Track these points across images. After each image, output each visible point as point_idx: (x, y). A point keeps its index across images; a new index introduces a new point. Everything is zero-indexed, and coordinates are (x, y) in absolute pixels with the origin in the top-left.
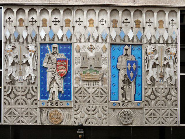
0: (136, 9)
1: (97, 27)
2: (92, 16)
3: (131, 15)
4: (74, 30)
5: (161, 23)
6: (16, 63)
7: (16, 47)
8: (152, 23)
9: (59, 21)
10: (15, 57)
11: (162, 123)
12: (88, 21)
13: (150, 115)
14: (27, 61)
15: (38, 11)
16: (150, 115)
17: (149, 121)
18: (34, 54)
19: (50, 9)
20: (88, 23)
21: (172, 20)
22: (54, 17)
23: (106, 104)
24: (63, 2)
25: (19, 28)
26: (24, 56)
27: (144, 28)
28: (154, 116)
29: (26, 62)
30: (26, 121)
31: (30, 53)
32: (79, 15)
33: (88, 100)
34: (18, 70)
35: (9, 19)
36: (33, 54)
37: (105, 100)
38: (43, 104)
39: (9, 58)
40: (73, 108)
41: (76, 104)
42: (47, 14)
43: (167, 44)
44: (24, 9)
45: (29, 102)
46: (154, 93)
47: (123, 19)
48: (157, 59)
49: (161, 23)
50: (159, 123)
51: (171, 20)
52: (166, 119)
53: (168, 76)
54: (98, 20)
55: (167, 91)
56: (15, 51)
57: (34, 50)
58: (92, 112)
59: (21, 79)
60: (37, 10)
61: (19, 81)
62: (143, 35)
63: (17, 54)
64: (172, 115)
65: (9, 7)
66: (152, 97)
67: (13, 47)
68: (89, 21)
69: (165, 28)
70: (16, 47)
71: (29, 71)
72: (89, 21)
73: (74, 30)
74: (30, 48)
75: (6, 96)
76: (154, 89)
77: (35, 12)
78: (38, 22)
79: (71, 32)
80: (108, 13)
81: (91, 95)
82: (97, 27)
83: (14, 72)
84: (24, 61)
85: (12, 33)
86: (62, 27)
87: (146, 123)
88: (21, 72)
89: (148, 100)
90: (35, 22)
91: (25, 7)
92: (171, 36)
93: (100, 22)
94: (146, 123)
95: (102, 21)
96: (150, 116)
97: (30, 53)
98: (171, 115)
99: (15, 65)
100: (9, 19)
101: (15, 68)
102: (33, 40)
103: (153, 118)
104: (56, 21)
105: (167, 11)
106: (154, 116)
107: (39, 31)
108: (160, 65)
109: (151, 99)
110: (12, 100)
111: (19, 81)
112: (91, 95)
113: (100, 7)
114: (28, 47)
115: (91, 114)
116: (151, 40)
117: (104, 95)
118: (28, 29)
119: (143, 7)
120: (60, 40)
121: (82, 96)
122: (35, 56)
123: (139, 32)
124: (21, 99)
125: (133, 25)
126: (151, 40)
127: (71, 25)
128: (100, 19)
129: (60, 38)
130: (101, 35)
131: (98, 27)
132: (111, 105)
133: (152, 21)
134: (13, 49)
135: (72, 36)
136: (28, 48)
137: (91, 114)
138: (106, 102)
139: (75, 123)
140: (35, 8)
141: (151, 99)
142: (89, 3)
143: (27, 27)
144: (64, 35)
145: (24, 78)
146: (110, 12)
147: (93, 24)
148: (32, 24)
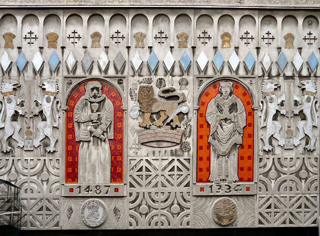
0: (309, 14)
1: (237, 48)
2: (96, 27)
3: (171, 23)
4: (63, 53)
5: (226, 37)
6: (21, 115)
7: (20, 86)
8: (166, 38)
9: (315, 39)
10: (18, 105)
11: (291, 222)
12: (219, 37)
13: (298, 208)
14: (41, 112)
15: (107, 17)
16: (298, 208)
17: (296, 218)
18: (55, 98)
19: (237, 14)
20: (284, 41)
21: (310, 34)
22: (267, 28)
23: (188, 189)
24: (290, 4)
25: (287, 52)
26: (35, 103)
27: (300, 49)
28: (276, 210)
29: (39, 113)
30: (37, 223)
31: (46, 96)
32: (74, 27)
33: (154, 182)
34: (25, 129)
35: (31, 35)
36: (52, 98)
37: (185, 183)
38: (202, 189)
39: (7, 107)
40: (255, 196)
41: (133, 189)
42: (37, 25)
43: (301, 77)
44: (189, 15)
45: (273, 185)
46: (275, 167)
47: (156, 32)
48: (282, 104)
49: (226, 37)
50: (284, 222)
51: (159, 33)
52: (296, 215)
53: (302, 135)
54: (22, 34)
55: (299, 163)
56: (278, 93)
57: (53, 90)
58: (163, 204)
59: (29, 145)
60: (61, 18)
61: (25, 149)
62: (192, 61)
63: (283, 98)
64: (308, 208)
65: (140, 12)
66: (273, 174)
67: (14, 85)
68: (285, 38)
69: (189, 46)
70: (20, 86)
71: (45, 129)
72: (285, 38)
73: (63, 53)
74: (48, 87)
75: (261, 176)
76: (276, 161)
77: (13, 21)
78: (194, 37)
79: (124, 56)
80: (127, 20)
81: (160, 173)
82: (237, 48)
83: (17, 132)
84: (37, 111)
85: (14, 61)
86: (41, 48)
87: (260, 222)
88: (30, 131)
89: (264, 179)
90: (201, 36)
91: (275, 12)
92: (244, 62)
93: (113, 38)
94: (260, 222)
95: (115, 35)
96: (268, 210)
97: (46, 96)
98: (306, 207)
99: (19, 118)
100: (31, 35)
101: (17, 125)
102: (4, 75)
103: (303, 212)
104: (161, 37)
105: (281, 16)
106: (276, 210)
107: (194, 55)
108: (287, 115)
109: (301, 179)
110: (303, 181)
111: (27, 149)
112: (160, 173)
113: (114, 10)
114: (44, 85)
115: (160, 208)
116: (270, 69)
117: (185, 172)
118: (110, 51)
119: (127, 9)
120: (38, 72)
121: (176, 175)
122: (55, 102)
123: (120, 55)
124: (288, 180)
125: (174, 42)
126: (270, 69)
127: (60, 44)
128: (242, 34)
129: (70, 68)
130: (244, 62)
131: (43, 48)
132: (65, 192)
133: (209, 34)
134: (14, 89)
135: (61, 66)
136: (44, 87)
137: (160, 208)
138: (188, 185)
139: (131, 225)
140: (36, 13)
141: (301, 179)
142: (25, 4)
143: (106, 47)
144: (46, 61)
145: (37, 143)
146: (260, 19)
147: (229, 42)
148: (29, 43)
